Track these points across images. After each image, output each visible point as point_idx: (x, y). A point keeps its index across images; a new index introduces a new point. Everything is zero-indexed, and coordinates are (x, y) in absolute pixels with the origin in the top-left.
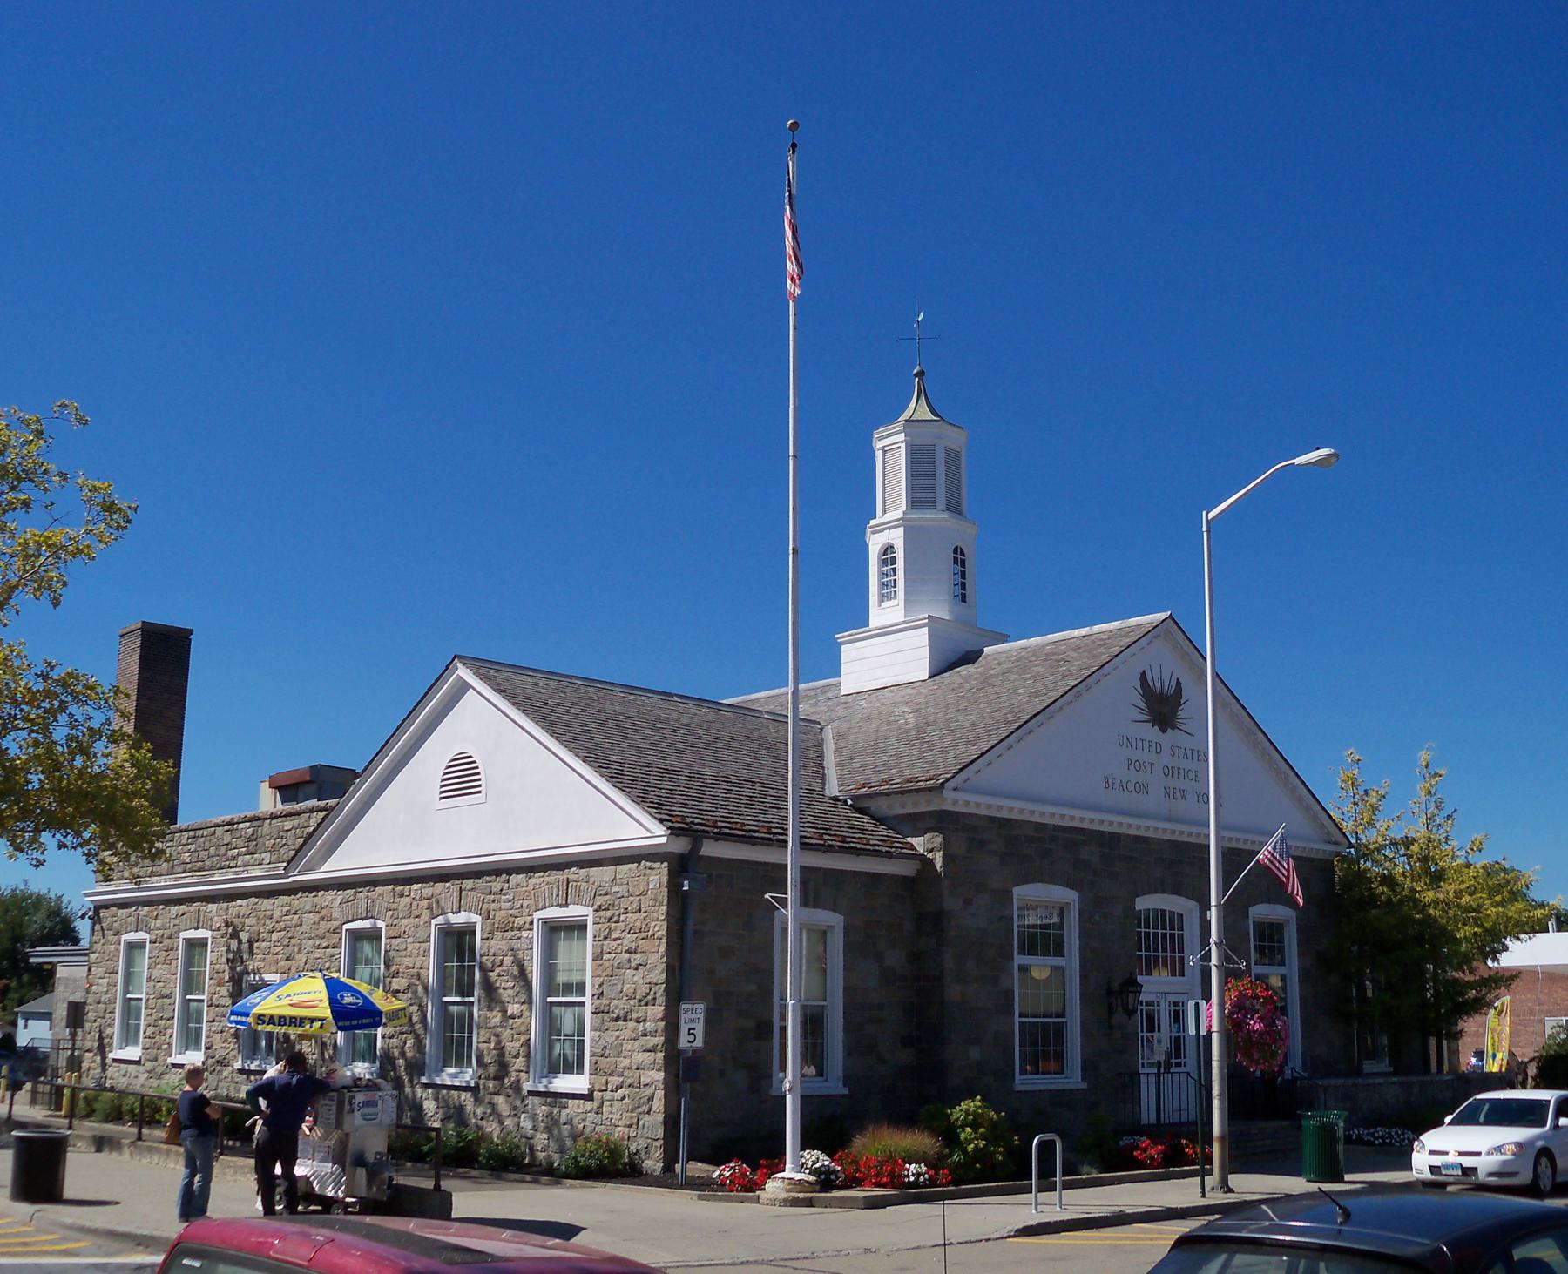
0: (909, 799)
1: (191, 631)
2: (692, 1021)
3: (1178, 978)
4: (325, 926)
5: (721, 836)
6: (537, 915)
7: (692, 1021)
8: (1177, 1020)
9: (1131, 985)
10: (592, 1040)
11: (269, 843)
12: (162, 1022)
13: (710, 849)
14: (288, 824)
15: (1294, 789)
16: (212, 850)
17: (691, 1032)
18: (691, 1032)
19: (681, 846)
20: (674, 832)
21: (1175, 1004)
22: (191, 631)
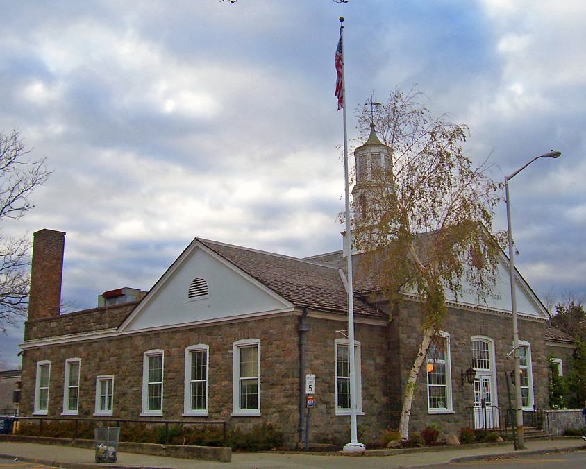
0: (154, 418)
1: (65, 233)
2: (310, 382)
3: (486, 370)
4: (135, 353)
5: (314, 310)
6: (234, 343)
7: (310, 382)
8: (486, 386)
9: (471, 372)
10: (261, 394)
11: (108, 320)
12: (58, 398)
13: (310, 314)
14: (117, 311)
15: (528, 294)
16: (81, 324)
17: (310, 386)
18: (310, 386)
19: (299, 312)
20: (297, 307)
21: (486, 380)
22: (65, 233)
